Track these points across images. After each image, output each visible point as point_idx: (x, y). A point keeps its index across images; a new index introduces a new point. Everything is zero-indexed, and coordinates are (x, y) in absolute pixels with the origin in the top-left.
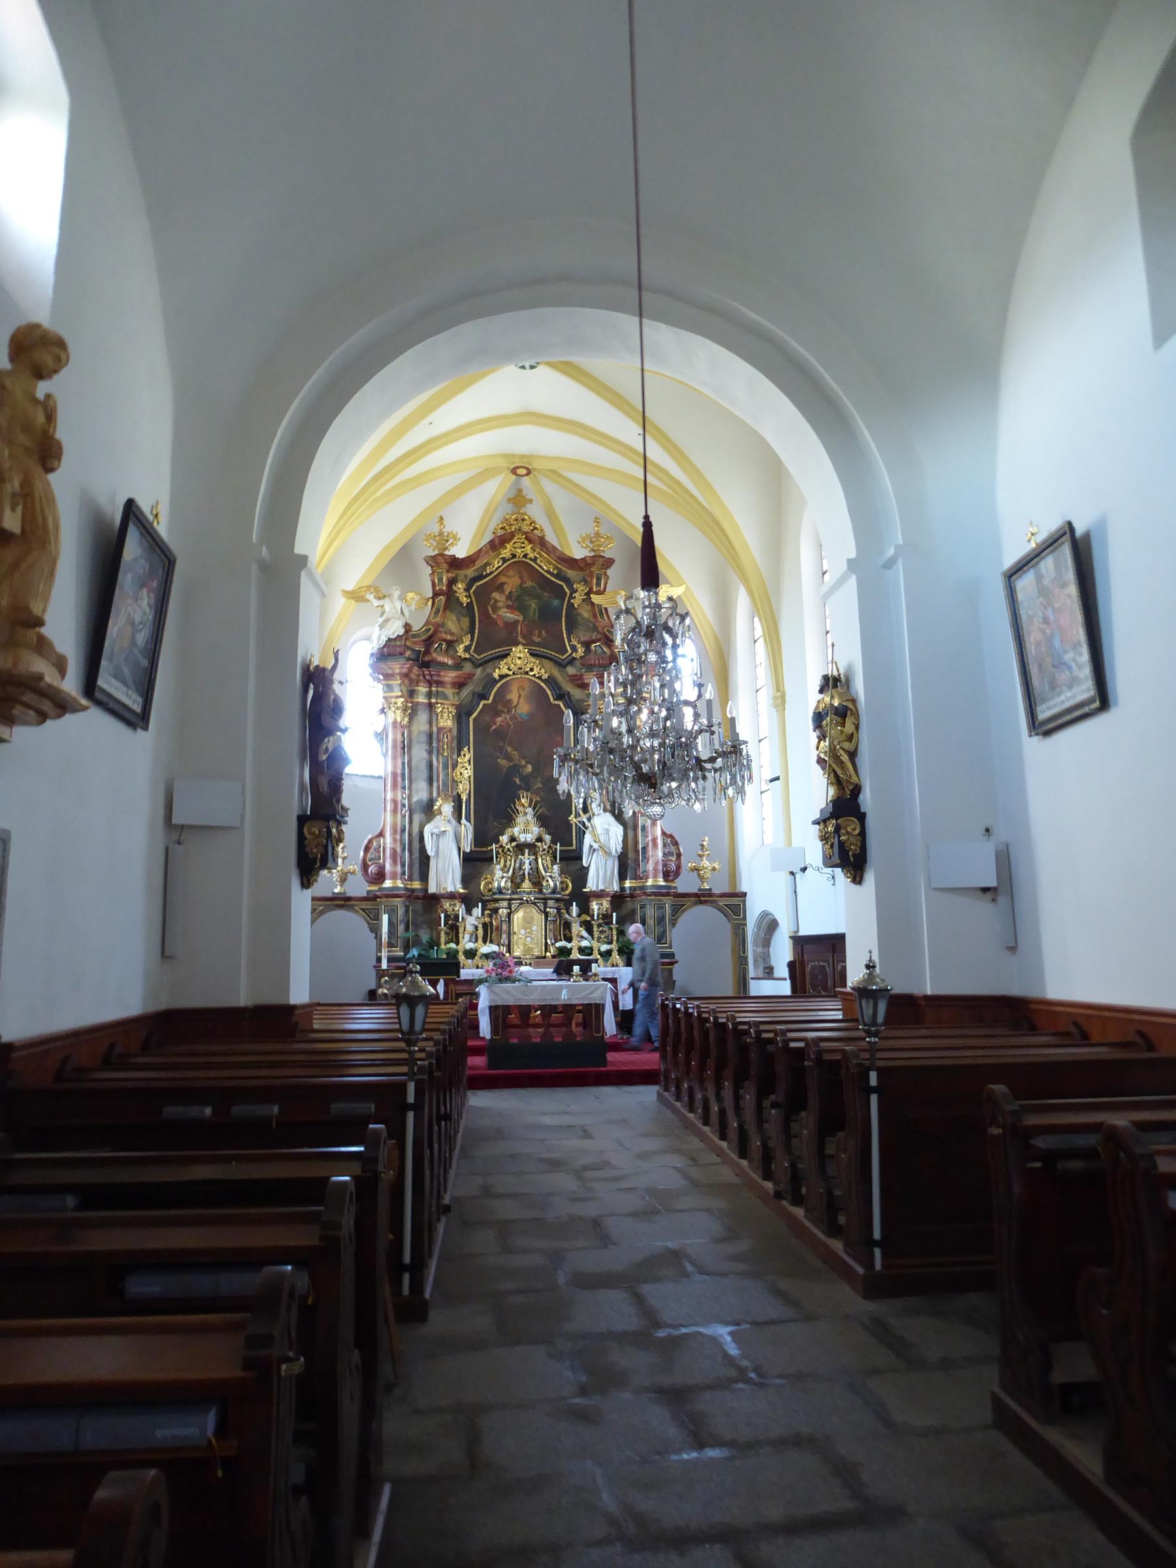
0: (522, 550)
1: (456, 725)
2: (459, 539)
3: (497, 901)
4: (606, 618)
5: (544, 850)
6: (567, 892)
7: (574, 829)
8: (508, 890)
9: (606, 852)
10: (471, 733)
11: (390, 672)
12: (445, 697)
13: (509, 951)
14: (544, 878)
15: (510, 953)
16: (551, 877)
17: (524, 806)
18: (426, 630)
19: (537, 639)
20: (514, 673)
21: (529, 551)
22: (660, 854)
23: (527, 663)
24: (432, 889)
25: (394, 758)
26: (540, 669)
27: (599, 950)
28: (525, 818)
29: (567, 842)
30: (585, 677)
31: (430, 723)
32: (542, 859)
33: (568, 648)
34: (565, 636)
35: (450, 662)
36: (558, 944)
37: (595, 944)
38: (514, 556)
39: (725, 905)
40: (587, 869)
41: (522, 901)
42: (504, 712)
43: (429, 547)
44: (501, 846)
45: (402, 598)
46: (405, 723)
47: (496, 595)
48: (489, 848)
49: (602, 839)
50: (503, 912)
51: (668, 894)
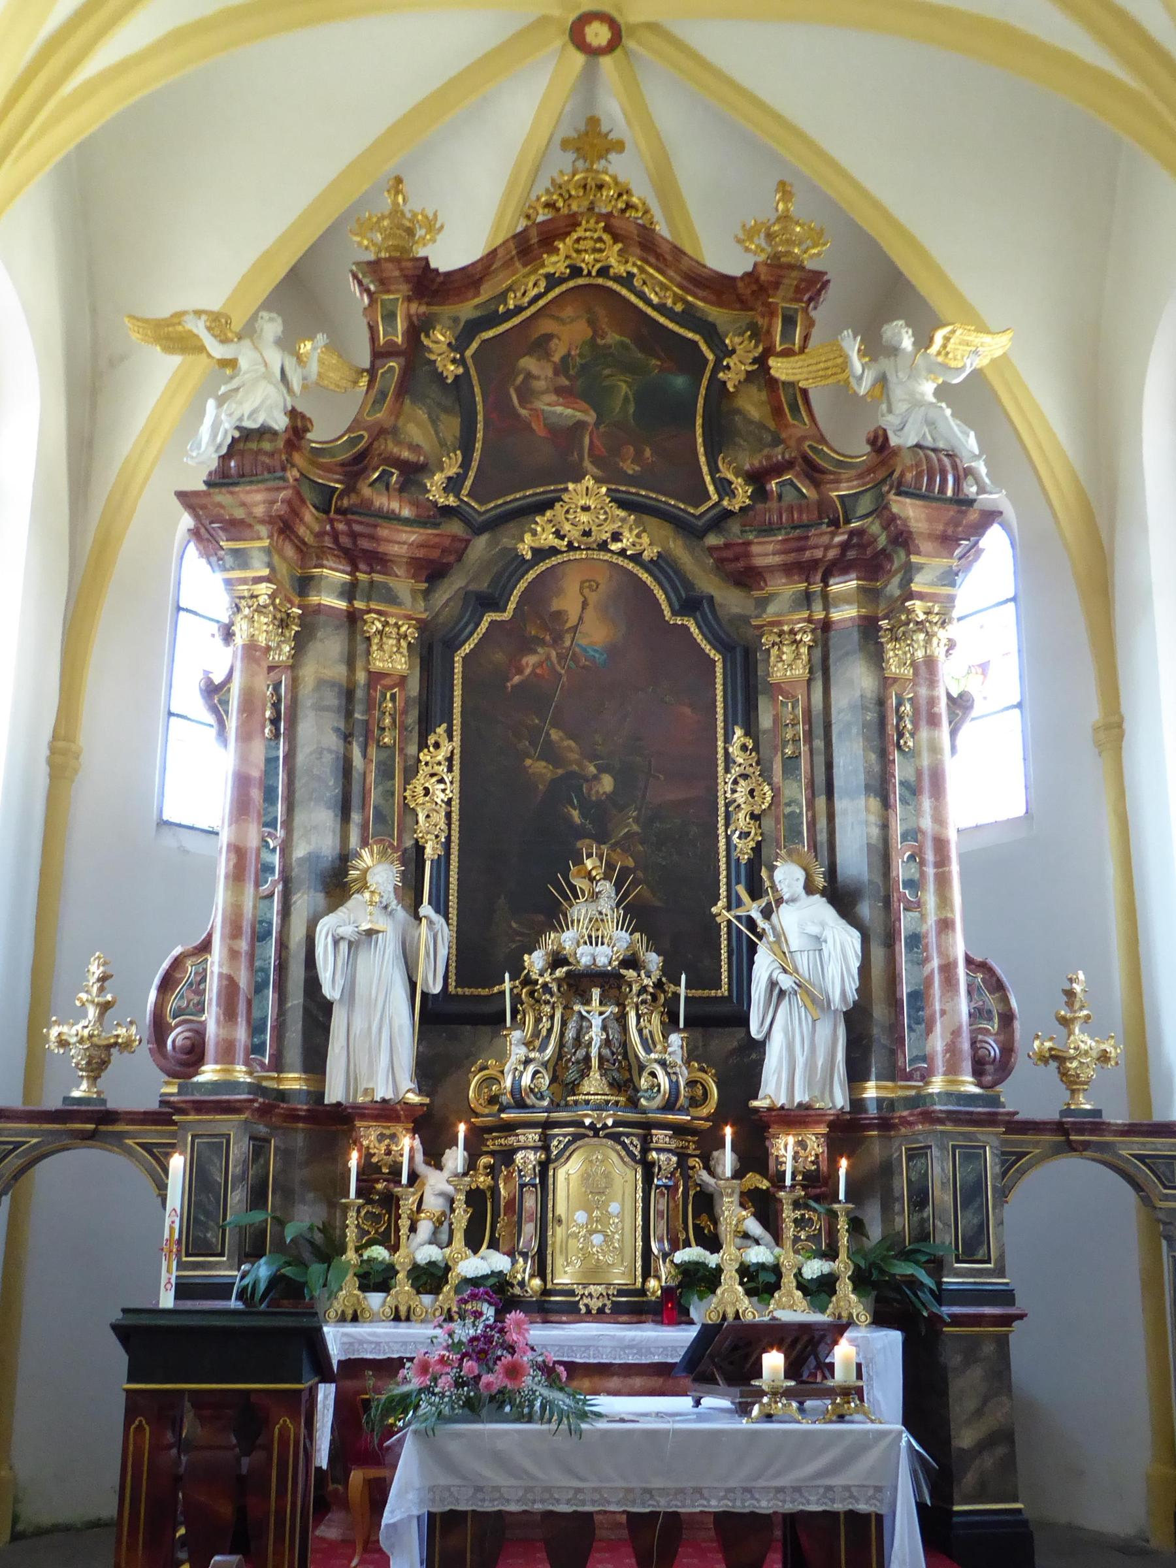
0: (597, 256)
1: (418, 669)
2: (442, 227)
3: (509, 1128)
4: (806, 419)
5: (644, 989)
6: (705, 1111)
7: (724, 936)
8: (542, 1098)
9: (814, 1000)
10: (458, 692)
11: (239, 514)
12: (392, 598)
13: (541, 1271)
14: (642, 1068)
15: (544, 1279)
16: (663, 1064)
17: (592, 879)
18: (350, 440)
19: (630, 468)
20: (570, 544)
21: (613, 261)
22: (963, 1007)
23: (606, 520)
24: (335, 1093)
25: (245, 736)
26: (638, 536)
27: (799, 1274)
28: (593, 906)
29: (704, 978)
30: (755, 549)
31: (350, 663)
32: (639, 1017)
33: (711, 488)
34: (702, 459)
35: (406, 512)
36: (680, 1256)
37: (788, 1259)
38: (576, 272)
39: (1141, 1158)
40: (760, 1047)
41: (582, 1130)
42: (542, 642)
43: (367, 248)
44: (528, 981)
45: (287, 343)
46: (283, 658)
47: (528, 363)
48: (496, 990)
49: (803, 962)
50: (526, 1159)
51: (990, 1120)
